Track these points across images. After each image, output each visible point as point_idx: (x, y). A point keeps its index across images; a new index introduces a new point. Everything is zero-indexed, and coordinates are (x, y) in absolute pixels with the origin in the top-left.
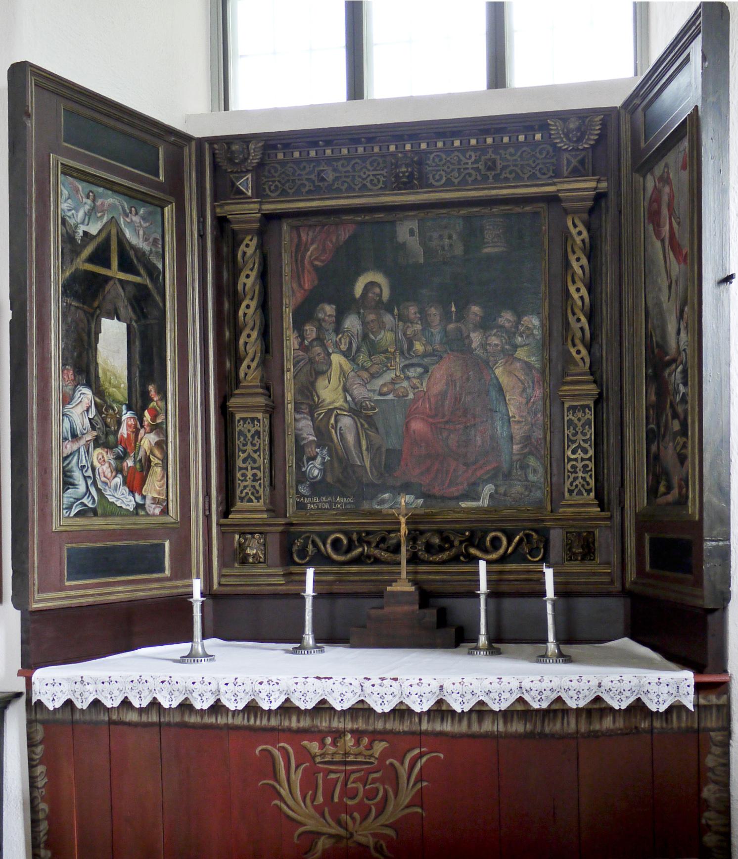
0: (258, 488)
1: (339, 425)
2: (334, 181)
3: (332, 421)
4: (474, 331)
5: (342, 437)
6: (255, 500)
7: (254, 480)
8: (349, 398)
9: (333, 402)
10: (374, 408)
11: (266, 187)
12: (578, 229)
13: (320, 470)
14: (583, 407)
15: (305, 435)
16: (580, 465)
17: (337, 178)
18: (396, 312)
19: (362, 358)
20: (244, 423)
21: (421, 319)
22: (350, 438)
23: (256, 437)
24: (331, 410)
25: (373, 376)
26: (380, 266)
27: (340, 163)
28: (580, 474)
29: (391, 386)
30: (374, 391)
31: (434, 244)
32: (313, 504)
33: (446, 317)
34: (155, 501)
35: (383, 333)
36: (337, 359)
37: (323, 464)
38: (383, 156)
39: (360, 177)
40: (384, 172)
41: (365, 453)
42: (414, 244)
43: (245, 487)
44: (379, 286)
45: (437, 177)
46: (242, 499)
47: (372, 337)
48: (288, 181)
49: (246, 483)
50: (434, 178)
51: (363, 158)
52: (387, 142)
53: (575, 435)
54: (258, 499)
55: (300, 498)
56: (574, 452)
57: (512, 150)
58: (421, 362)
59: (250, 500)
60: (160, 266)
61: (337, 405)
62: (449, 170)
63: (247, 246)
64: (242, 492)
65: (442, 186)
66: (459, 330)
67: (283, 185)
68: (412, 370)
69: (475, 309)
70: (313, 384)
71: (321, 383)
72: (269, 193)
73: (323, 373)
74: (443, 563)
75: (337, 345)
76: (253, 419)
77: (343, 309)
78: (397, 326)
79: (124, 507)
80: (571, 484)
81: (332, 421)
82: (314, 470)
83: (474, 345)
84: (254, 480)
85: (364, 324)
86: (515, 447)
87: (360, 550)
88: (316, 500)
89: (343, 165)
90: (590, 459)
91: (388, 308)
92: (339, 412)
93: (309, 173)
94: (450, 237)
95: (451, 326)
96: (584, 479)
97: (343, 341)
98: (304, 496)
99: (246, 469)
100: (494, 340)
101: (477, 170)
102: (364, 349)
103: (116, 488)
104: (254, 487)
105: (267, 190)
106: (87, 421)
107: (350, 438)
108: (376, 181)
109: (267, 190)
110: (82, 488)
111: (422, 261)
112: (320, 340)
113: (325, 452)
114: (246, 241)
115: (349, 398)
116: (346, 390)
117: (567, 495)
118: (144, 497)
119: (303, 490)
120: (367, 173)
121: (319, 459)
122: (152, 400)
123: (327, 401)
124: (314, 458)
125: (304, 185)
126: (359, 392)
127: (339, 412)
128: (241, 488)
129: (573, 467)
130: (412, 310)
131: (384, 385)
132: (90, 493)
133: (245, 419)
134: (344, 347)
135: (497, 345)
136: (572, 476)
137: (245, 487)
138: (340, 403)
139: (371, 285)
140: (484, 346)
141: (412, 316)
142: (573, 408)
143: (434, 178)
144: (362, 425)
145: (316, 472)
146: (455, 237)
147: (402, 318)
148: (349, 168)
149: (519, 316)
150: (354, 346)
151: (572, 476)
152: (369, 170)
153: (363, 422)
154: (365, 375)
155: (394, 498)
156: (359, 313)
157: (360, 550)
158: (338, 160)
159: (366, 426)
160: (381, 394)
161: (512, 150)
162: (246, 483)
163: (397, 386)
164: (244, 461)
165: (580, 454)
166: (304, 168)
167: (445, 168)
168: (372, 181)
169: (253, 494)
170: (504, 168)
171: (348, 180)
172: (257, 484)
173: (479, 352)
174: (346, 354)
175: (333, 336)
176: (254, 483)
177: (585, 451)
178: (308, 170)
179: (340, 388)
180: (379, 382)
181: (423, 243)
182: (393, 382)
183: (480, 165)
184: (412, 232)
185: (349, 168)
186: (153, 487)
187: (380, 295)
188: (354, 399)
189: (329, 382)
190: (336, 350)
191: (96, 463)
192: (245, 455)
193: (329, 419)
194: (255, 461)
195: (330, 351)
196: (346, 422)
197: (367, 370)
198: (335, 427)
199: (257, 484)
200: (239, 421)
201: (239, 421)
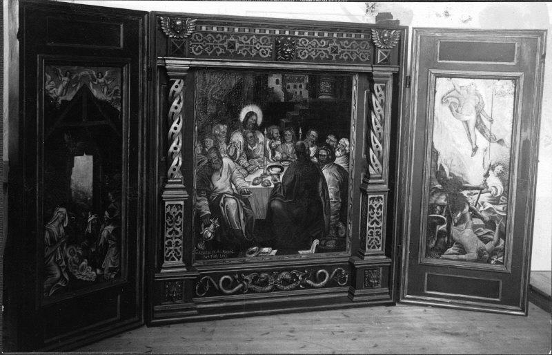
0: (179, 251)
1: (226, 204)
2: (238, 49)
3: (222, 201)
4: (312, 146)
5: (228, 211)
6: (177, 259)
7: (177, 246)
8: (233, 187)
9: (223, 189)
10: (249, 193)
11: (192, 48)
12: (379, 93)
13: (212, 233)
14: (378, 199)
15: (203, 211)
16: (375, 231)
17: (241, 48)
18: (265, 132)
19: (244, 162)
20: (171, 208)
21: (281, 137)
22: (233, 212)
23: (179, 217)
24: (223, 194)
25: (249, 173)
26: (255, 101)
27: (242, 38)
28: (375, 237)
29: (260, 180)
30: (249, 182)
31: (291, 90)
32: (207, 255)
33: (296, 138)
34: (111, 270)
35: (257, 145)
36: (226, 161)
37: (214, 229)
38: (271, 36)
39: (255, 48)
40: (271, 47)
41: (242, 221)
42: (278, 89)
43: (170, 250)
44: (256, 115)
45: (303, 54)
46: (167, 259)
47: (249, 147)
48: (208, 46)
49: (171, 248)
50: (301, 54)
51: (258, 36)
52: (274, 28)
53: (373, 214)
54: (179, 258)
55: (198, 252)
56: (372, 224)
57: (346, 42)
58: (280, 165)
59: (173, 259)
60: (119, 109)
61: (225, 191)
62: (310, 50)
63: (177, 87)
64: (167, 254)
65: (304, 61)
66: (303, 144)
67: (204, 48)
68: (274, 169)
69: (313, 133)
70: (210, 177)
71: (215, 176)
72: (195, 53)
73: (217, 170)
74: (291, 289)
75: (227, 152)
76: (177, 205)
77: (232, 129)
78: (266, 141)
79: (88, 279)
80: (370, 243)
81: (222, 201)
82: (208, 233)
83: (311, 155)
84: (177, 246)
85: (245, 137)
86: (332, 217)
87: (241, 285)
88: (209, 253)
89: (244, 39)
90: (380, 228)
91: (261, 129)
92: (227, 195)
93: (223, 42)
94: (301, 87)
95: (299, 142)
96: (376, 239)
97: (231, 149)
98: (201, 250)
99: (171, 238)
100: (323, 152)
101: (326, 51)
102: (244, 155)
103: (83, 269)
104: (176, 250)
105: (193, 50)
106: (62, 229)
107: (233, 212)
108: (265, 52)
109: (193, 50)
110: (58, 275)
111: (283, 101)
112: (216, 148)
113: (216, 221)
114: (176, 83)
115: (233, 187)
116: (232, 181)
117: (367, 248)
118: (102, 270)
119: (201, 246)
120: (260, 46)
121: (212, 226)
122: (110, 202)
123: (219, 188)
124: (209, 226)
125: (218, 50)
126: (240, 183)
127: (227, 195)
128: (167, 251)
129: (372, 232)
130: (275, 131)
131: (257, 179)
132: (64, 277)
133: (171, 206)
134: (231, 154)
135: (325, 155)
136: (370, 238)
137: (170, 250)
138: (228, 189)
139: (251, 114)
140: (317, 155)
141: (275, 135)
142: (373, 199)
143: (301, 54)
144: (241, 204)
145: (210, 235)
146: (303, 87)
147: (270, 136)
148: (249, 41)
149: (338, 139)
150: (238, 153)
151: (370, 238)
152: (261, 44)
153: (242, 202)
154: (245, 172)
155: (259, 249)
156: (242, 131)
157: (241, 285)
158: (241, 35)
159: (244, 204)
160: (254, 184)
161: (346, 42)
162: (171, 248)
163: (264, 179)
164: (170, 233)
165: (375, 225)
166: (244, 51)
167: (308, 48)
168: (263, 51)
169: (175, 255)
170: (342, 52)
171: (248, 49)
172: (178, 248)
173: (315, 160)
174: (232, 158)
175: (225, 146)
176: (176, 248)
177: (378, 223)
178: (221, 40)
179: (228, 180)
180: (252, 178)
181: (284, 89)
182: (262, 177)
183: (329, 49)
184: (277, 82)
185: (249, 41)
186: (109, 263)
187: (256, 120)
188: (236, 187)
189: (221, 176)
190: (226, 155)
191: (68, 255)
192: (171, 229)
193: (220, 199)
194: (177, 233)
195: (222, 156)
196: (232, 202)
197: (246, 169)
198: (223, 205)
199: (178, 248)
200: (167, 207)
201: (167, 207)
